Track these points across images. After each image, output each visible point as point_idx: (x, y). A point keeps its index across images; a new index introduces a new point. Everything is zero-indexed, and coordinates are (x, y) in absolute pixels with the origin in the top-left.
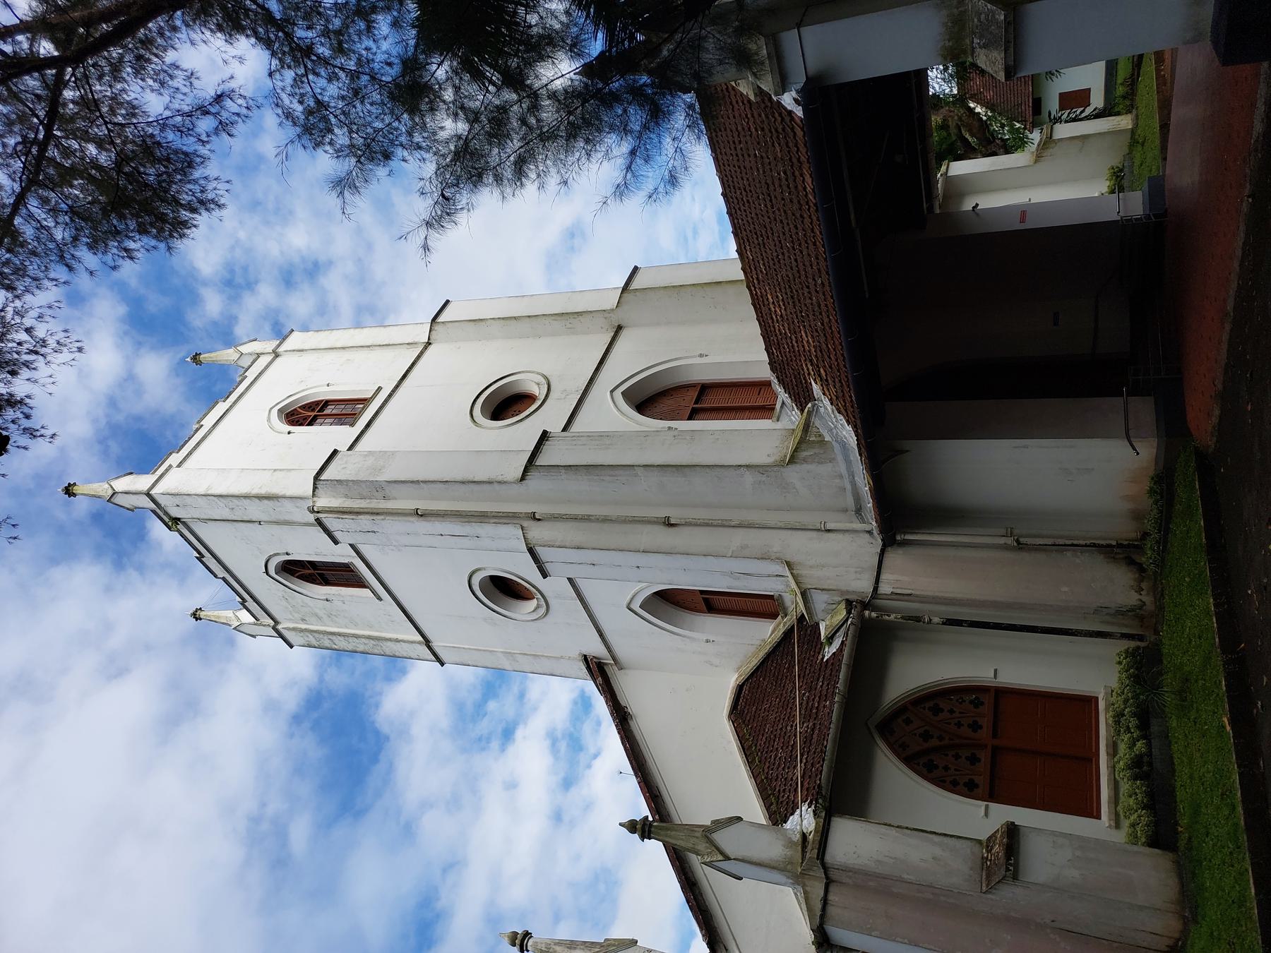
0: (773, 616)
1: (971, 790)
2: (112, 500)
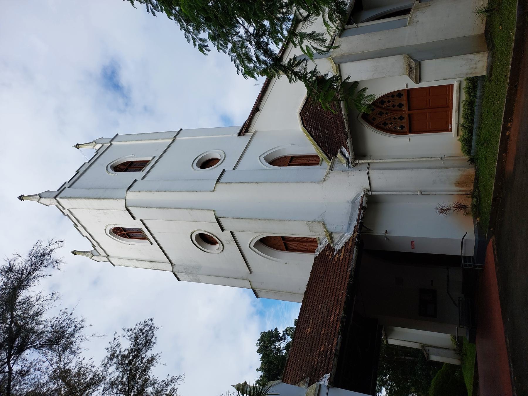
0: (313, 252)
1: (399, 93)
2: (39, 201)
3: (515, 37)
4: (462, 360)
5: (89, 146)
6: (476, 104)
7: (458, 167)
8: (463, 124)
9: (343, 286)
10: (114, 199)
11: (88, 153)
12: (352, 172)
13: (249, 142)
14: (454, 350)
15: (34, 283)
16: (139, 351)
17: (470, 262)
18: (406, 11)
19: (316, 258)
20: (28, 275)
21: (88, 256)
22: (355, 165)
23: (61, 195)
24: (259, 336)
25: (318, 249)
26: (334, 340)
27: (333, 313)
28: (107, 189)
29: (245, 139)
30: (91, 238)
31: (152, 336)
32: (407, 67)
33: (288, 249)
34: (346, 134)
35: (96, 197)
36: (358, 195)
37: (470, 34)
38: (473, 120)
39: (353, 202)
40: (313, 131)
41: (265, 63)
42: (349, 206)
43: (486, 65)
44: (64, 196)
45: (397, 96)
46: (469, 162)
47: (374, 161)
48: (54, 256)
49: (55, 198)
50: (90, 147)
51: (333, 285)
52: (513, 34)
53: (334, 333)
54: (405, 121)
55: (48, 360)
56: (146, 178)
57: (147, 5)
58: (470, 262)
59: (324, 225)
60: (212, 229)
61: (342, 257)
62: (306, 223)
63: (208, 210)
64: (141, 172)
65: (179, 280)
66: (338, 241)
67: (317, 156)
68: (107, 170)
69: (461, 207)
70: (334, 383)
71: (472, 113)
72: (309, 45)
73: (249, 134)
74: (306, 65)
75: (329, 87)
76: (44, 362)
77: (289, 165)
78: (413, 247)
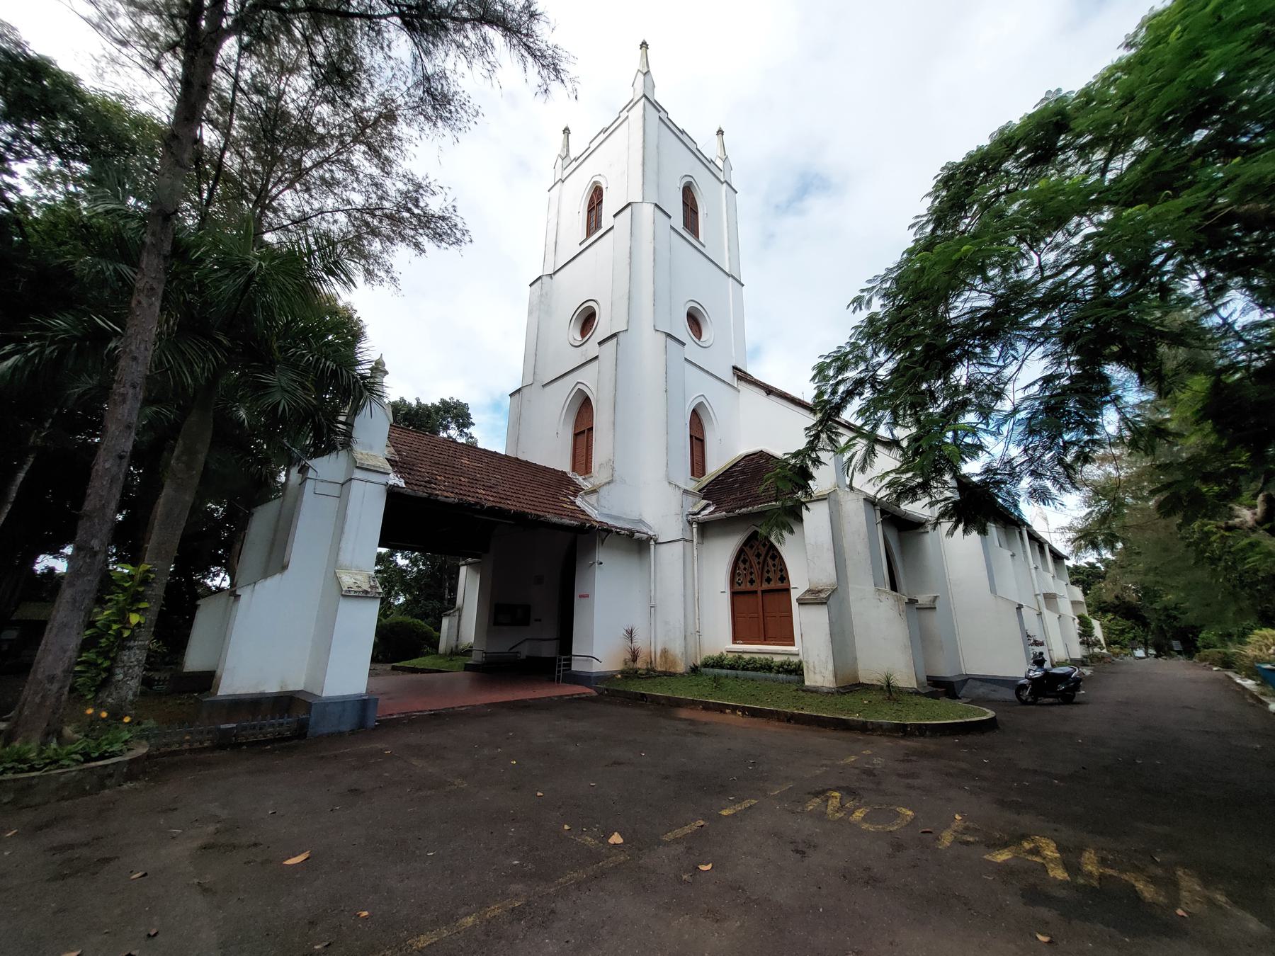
0: (574, 470)
1: (785, 579)
3: (853, 720)
4: (444, 655)
6: (767, 674)
7: (686, 653)
8: (742, 658)
9: (525, 506)
11: (710, 149)
12: (680, 519)
13: (724, 381)
14: (457, 646)
15: (515, 55)
16: (425, 225)
17: (564, 665)
18: (894, 587)
19: (565, 473)
20: (525, 44)
21: (562, 151)
22: (690, 523)
23: (647, 104)
24: (463, 401)
25: (578, 477)
26: (452, 492)
27: (488, 493)
29: (728, 376)
30: (588, 154)
31: (448, 243)
32: (820, 588)
33: (576, 435)
34: (732, 510)
36: (650, 528)
38: (747, 669)
39: (641, 521)
41: (834, 392)
42: (635, 516)
44: (647, 109)
45: (782, 576)
46: (692, 665)
47: (695, 548)
48: (555, 86)
49: (645, 96)
50: (719, 152)
51: (527, 494)
52: (856, 717)
53: (461, 494)
54: (749, 587)
55: (409, 89)
56: (672, 232)
57: (926, 215)
58: (564, 665)
59: (609, 483)
60: (602, 328)
61: (565, 505)
62: (612, 458)
63: (628, 322)
65: (531, 285)
66: (586, 502)
67: (704, 474)
68: (686, 176)
69: (635, 655)
70: (393, 495)
71: (755, 669)
72: (857, 448)
73: (735, 382)
74: (828, 451)
75: (797, 484)
76: (405, 83)
77: (691, 436)
78: (581, 596)
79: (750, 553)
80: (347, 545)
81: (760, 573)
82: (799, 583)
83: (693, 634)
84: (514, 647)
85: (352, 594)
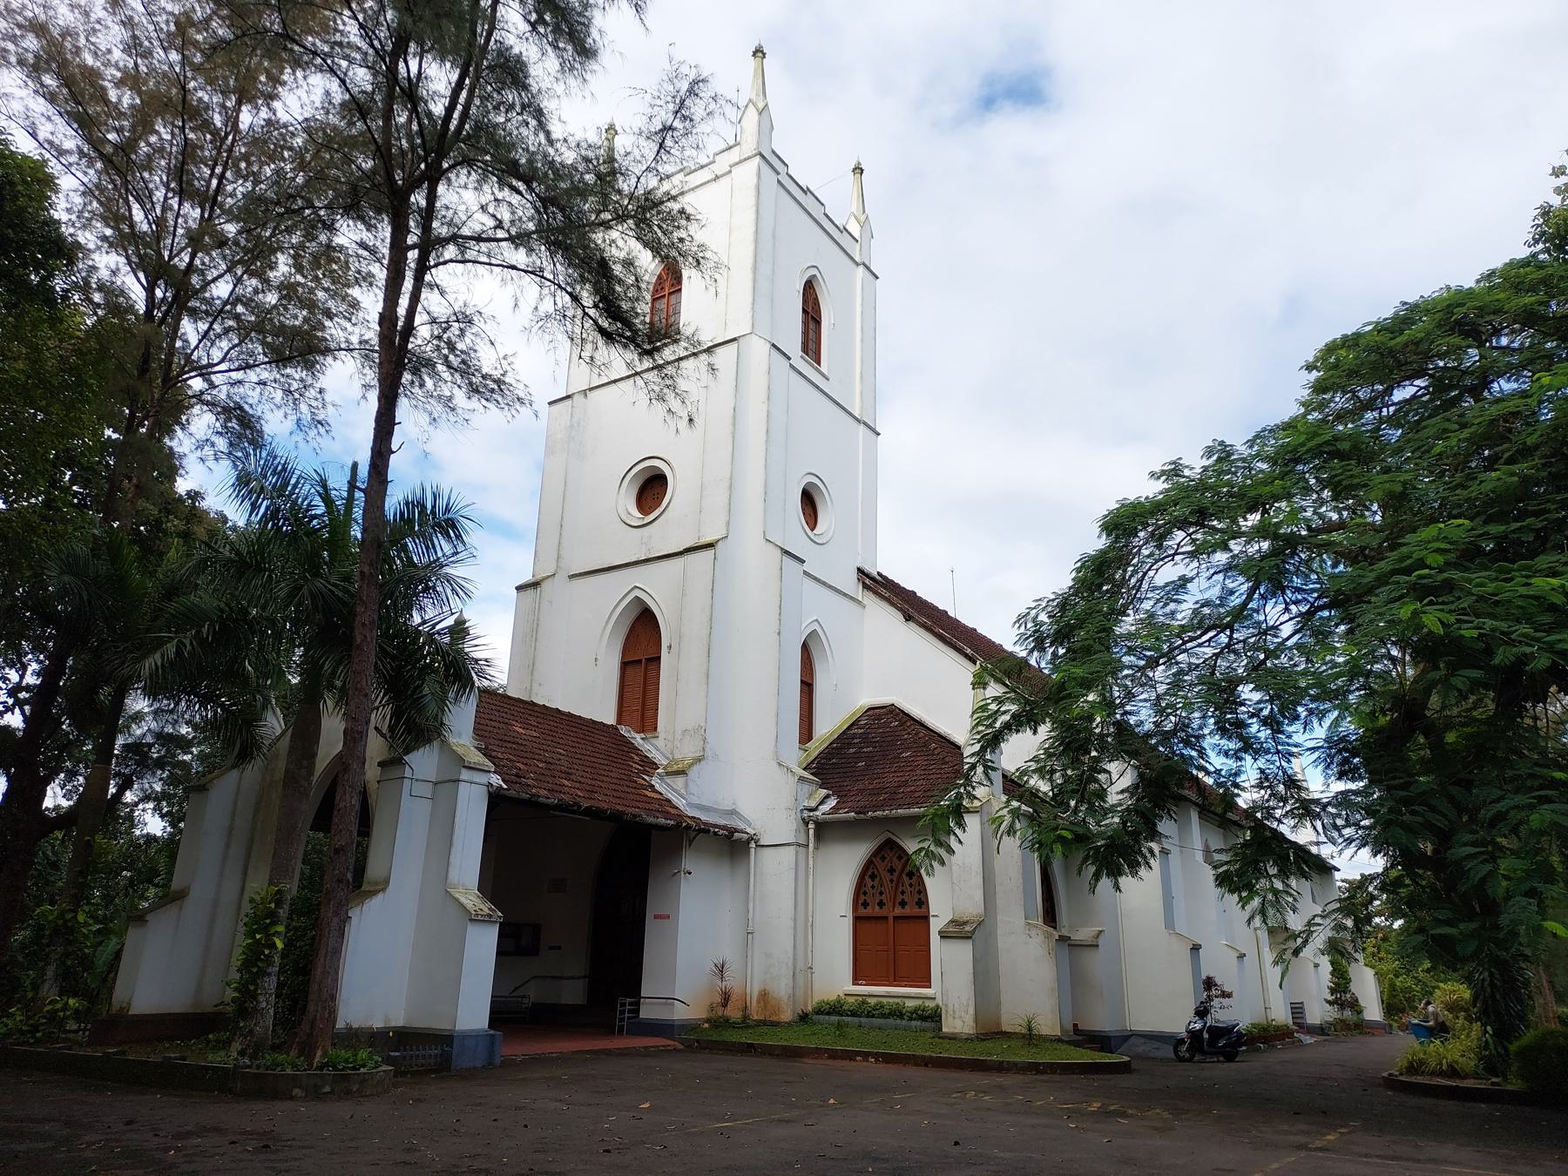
5: (858, 202)
6: (898, 1021)
7: (794, 995)
10: (753, 304)
11: (839, 202)
12: (793, 816)
13: (845, 595)
28: (727, 150)
29: (851, 585)
35: (758, 259)
37: (1004, 1010)
38: (873, 1016)
40: (860, 731)
42: (726, 805)
43: (956, 1031)
45: (920, 899)
46: (800, 1012)
50: (855, 207)
54: (877, 911)
63: (728, 524)
64: (801, 353)
69: (726, 998)
71: (883, 1016)
77: (802, 681)
79: (882, 867)
80: (455, 859)
81: (892, 893)
82: (941, 909)
83: (803, 970)
84: (516, 989)
85: (479, 918)
